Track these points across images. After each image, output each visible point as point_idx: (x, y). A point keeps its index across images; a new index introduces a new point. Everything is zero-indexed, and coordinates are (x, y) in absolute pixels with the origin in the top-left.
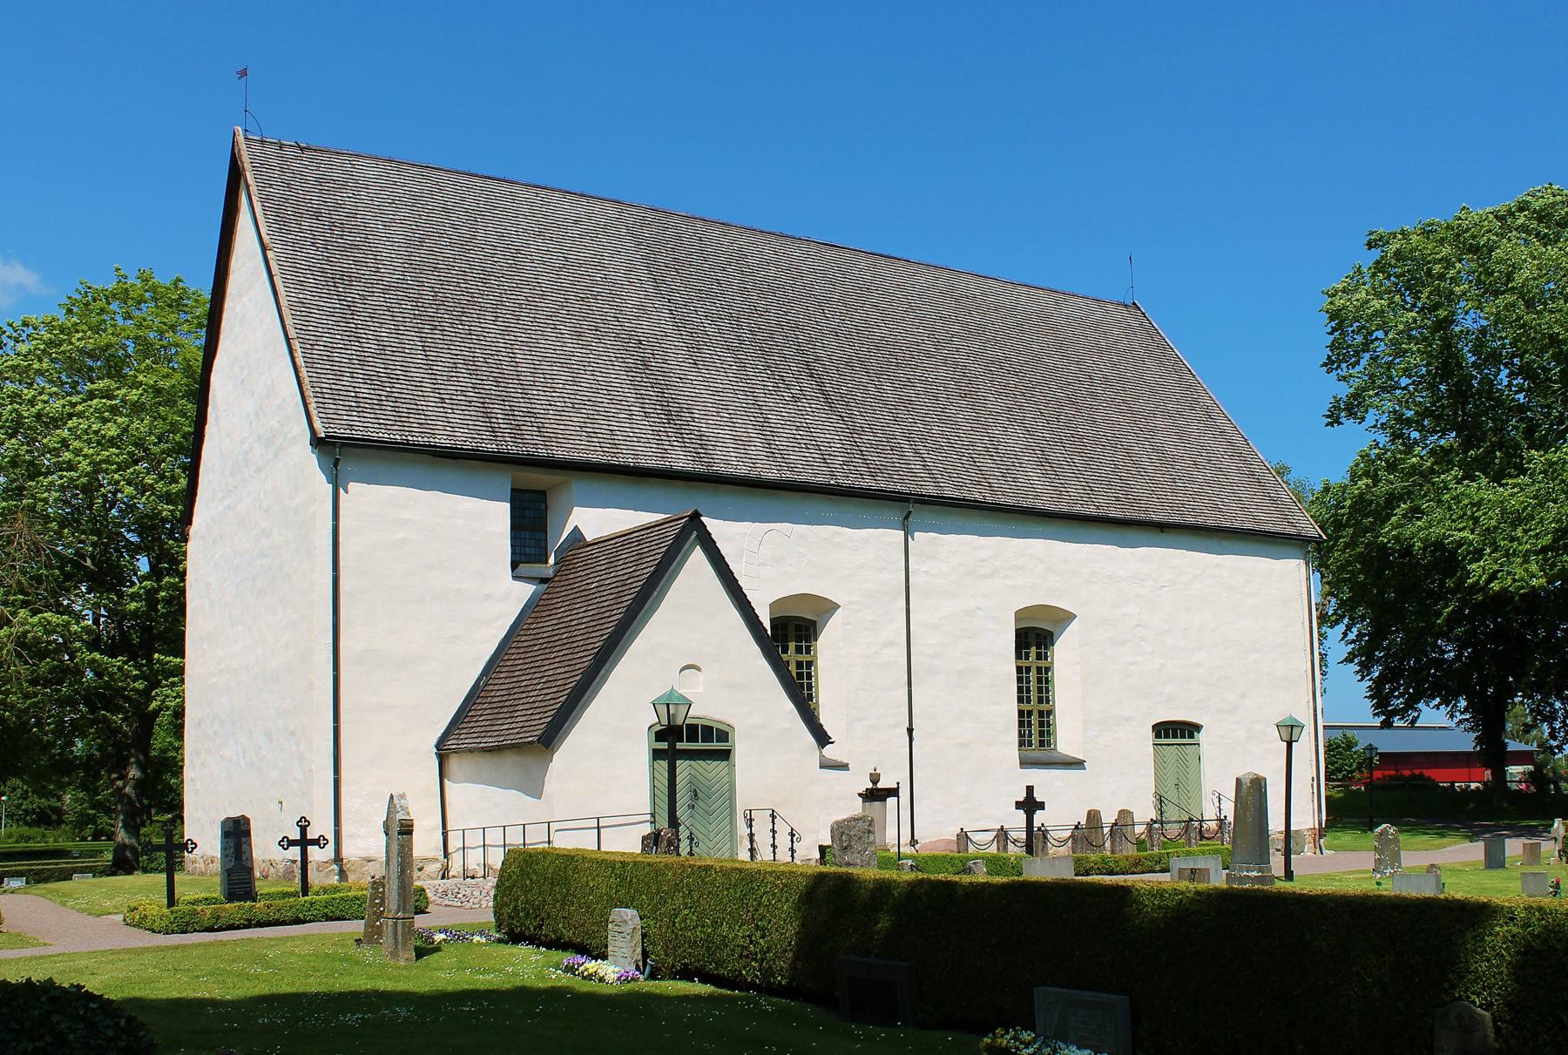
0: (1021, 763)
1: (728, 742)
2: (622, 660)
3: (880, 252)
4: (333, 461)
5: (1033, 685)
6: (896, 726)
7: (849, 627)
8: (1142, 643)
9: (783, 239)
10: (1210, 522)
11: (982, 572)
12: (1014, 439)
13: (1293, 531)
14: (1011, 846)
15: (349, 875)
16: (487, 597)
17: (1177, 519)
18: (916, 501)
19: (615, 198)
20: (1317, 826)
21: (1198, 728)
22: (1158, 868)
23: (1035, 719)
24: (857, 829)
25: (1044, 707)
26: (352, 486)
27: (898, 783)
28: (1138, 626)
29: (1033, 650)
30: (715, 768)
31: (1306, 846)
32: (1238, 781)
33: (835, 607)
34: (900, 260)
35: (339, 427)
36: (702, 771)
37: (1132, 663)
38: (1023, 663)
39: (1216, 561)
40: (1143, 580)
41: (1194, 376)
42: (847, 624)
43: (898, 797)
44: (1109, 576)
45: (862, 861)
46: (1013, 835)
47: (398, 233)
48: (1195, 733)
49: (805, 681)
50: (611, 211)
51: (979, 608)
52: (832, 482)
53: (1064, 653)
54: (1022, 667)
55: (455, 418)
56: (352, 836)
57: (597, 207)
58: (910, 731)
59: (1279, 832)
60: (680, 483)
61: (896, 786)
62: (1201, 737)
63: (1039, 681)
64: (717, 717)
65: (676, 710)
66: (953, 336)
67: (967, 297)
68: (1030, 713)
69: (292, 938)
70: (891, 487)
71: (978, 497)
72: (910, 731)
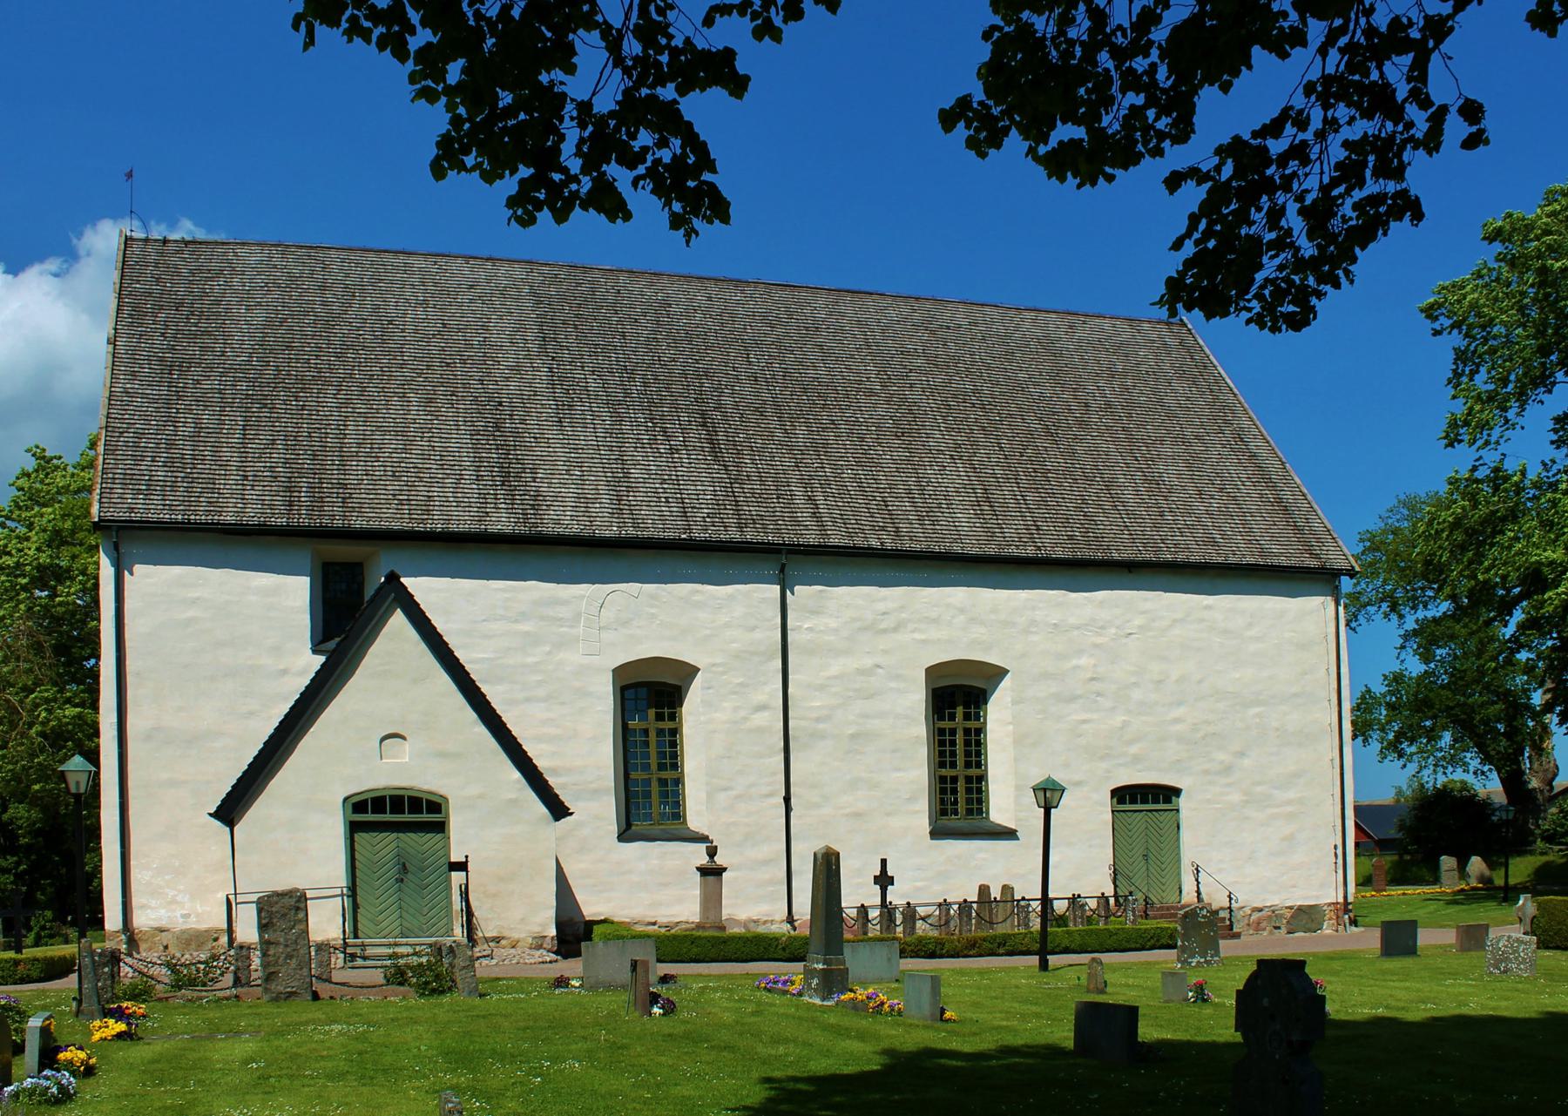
0: (931, 833)
1: (440, 813)
2: (312, 730)
3: (848, 288)
4: (112, 545)
5: (960, 748)
6: (770, 795)
7: (711, 691)
8: (1098, 698)
9: (725, 283)
10: (1195, 558)
11: (883, 626)
12: (957, 475)
13: (1313, 563)
14: (919, 923)
15: (140, 944)
16: (285, 672)
17: (1149, 556)
18: (790, 552)
19: (527, 257)
20: (1341, 900)
21: (1176, 792)
22: (1001, 951)
23: (961, 786)
24: (280, 904)
25: (973, 772)
26: (138, 568)
27: (467, 857)
28: (1093, 679)
29: (960, 711)
30: (427, 840)
31: (1325, 923)
32: (815, 854)
33: (690, 671)
34: (871, 294)
35: (118, 510)
36: (412, 843)
37: (1084, 722)
38: (946, 724)
39: (1205, 602)
40: (1102, 628)
41: (1235, 395)
42: (709, 688)
43: (467, 872)
44: (1055, 624)
45: (286, 940)
46: (921, 911)
47: (259, 316)
48: (1174, 798)
49: (974, 758)
50: (519, 271)
51: (878, 666)
52: (683, 536)
53: (999, 715)
54: (970, 729)
55: (251, 495)
56: (143, 907)
57: (503, 269)
58: (787, 799)
59: (1287, 908)
60: (505, 547)
61: (464, 860)
62: (1183, 802)
63: (967, 743)
64: (426, 787)
65: (1052, 796)
66: (911, 371)
67: (948, 328)
68: (954, 779)
69: (1015, 969)
70: (761, 537)
71: (875, 543)
72: (787, 799)
